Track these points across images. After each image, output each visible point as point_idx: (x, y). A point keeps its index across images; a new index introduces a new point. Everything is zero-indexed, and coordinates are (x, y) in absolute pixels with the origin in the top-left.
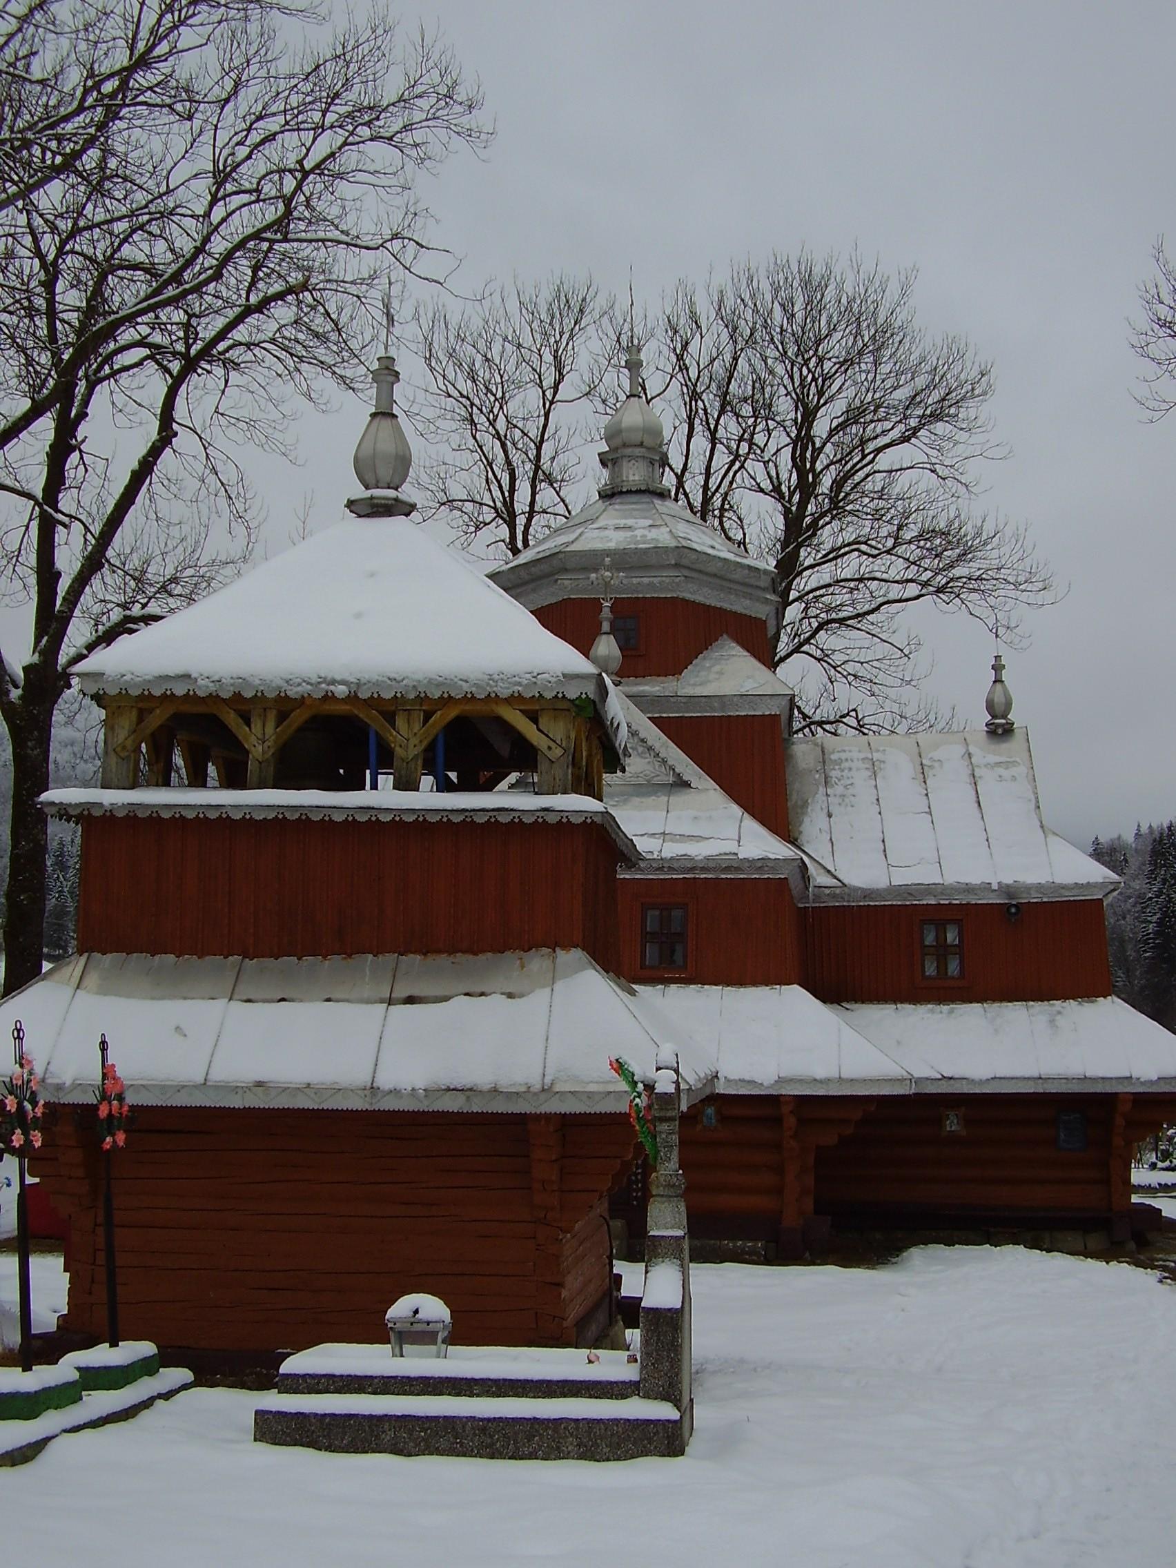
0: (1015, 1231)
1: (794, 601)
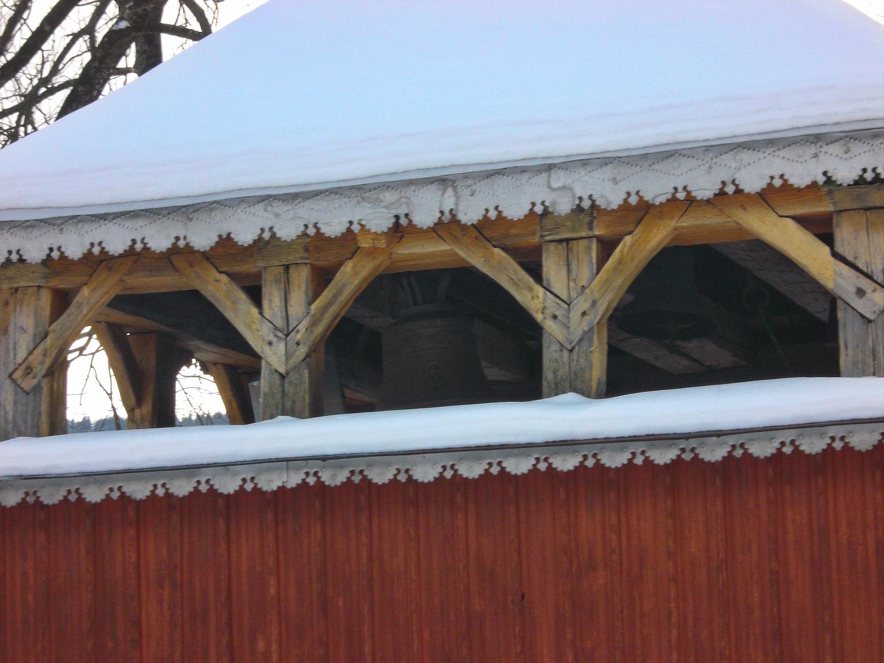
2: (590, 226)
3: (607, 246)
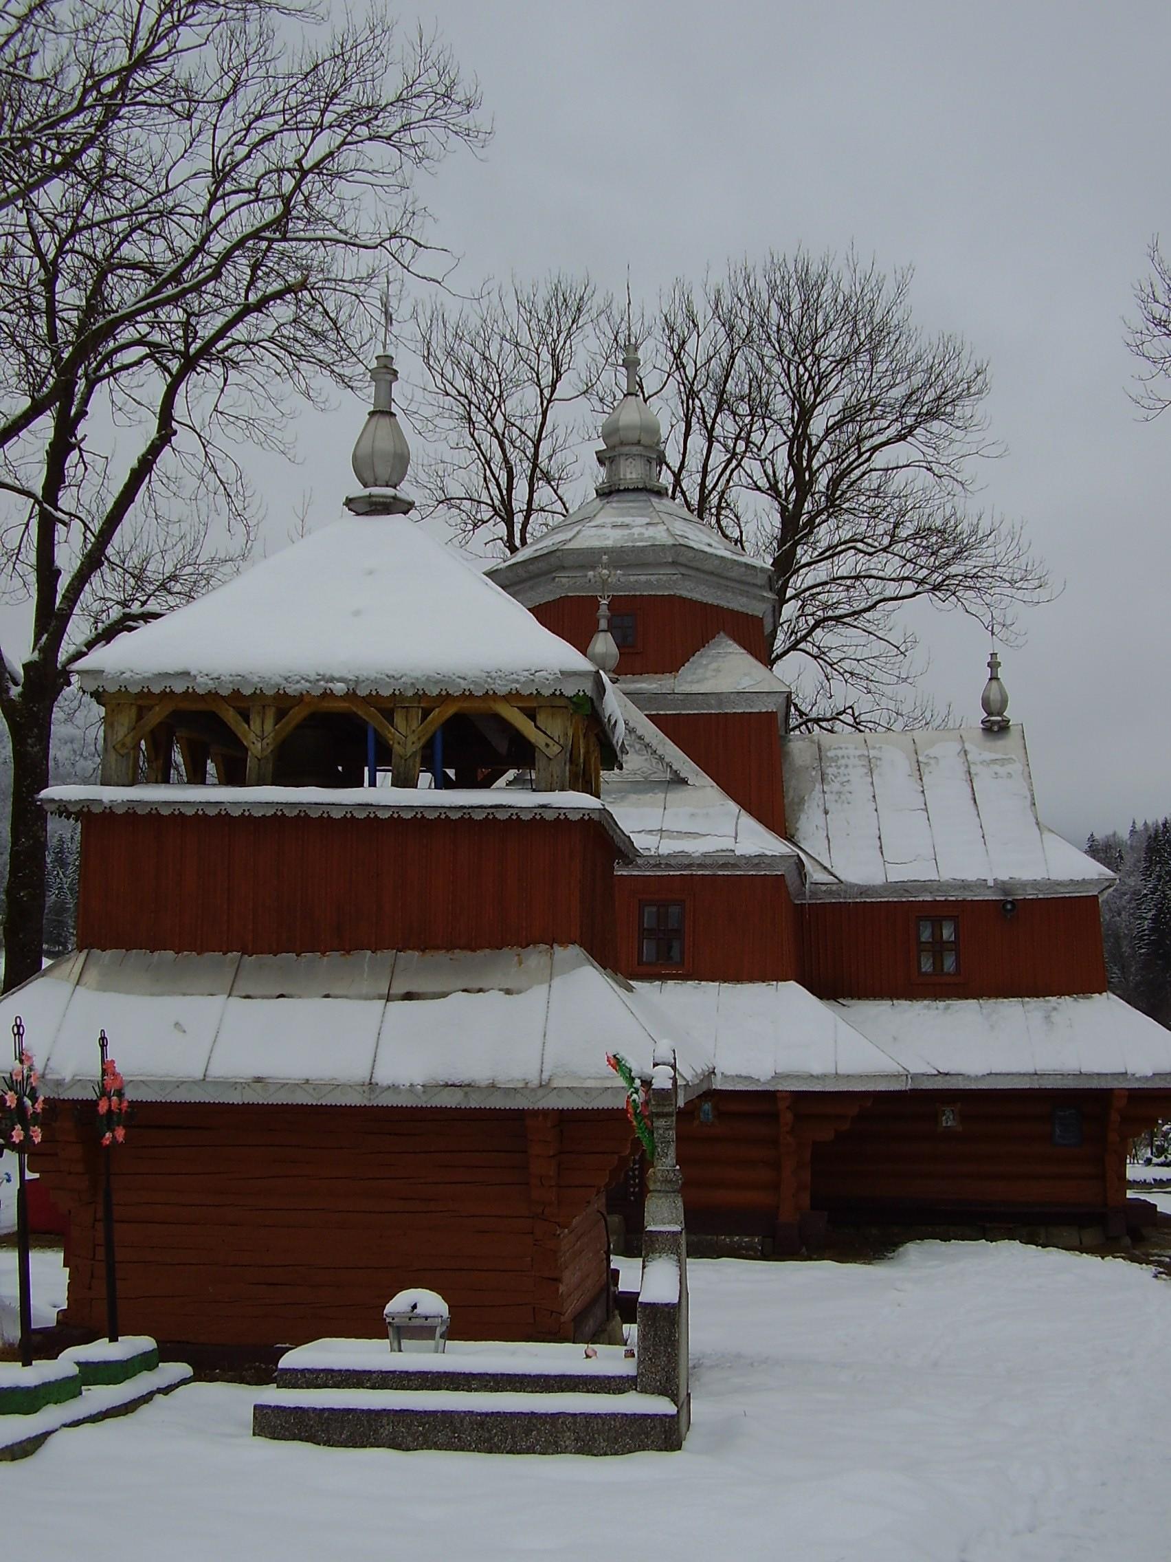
0: (1011, 1226)
1: (790, 599)
2: (419, 703)
3: (426, 713)
